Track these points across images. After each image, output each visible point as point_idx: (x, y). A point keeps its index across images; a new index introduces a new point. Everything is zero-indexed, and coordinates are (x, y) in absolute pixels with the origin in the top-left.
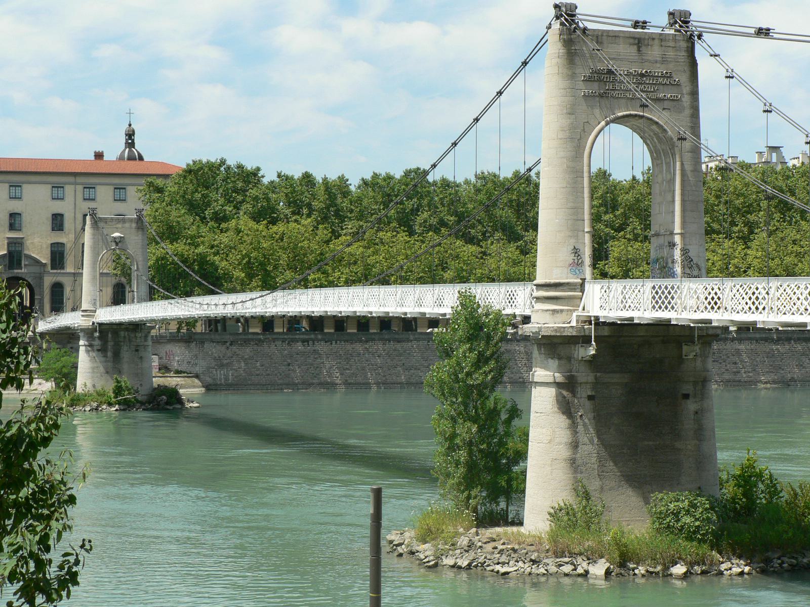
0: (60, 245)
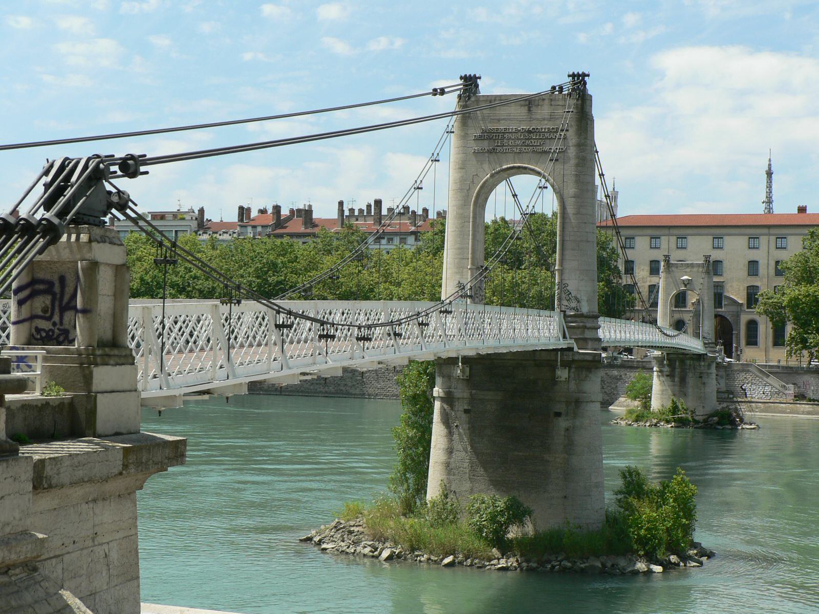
0: (755, 288)
